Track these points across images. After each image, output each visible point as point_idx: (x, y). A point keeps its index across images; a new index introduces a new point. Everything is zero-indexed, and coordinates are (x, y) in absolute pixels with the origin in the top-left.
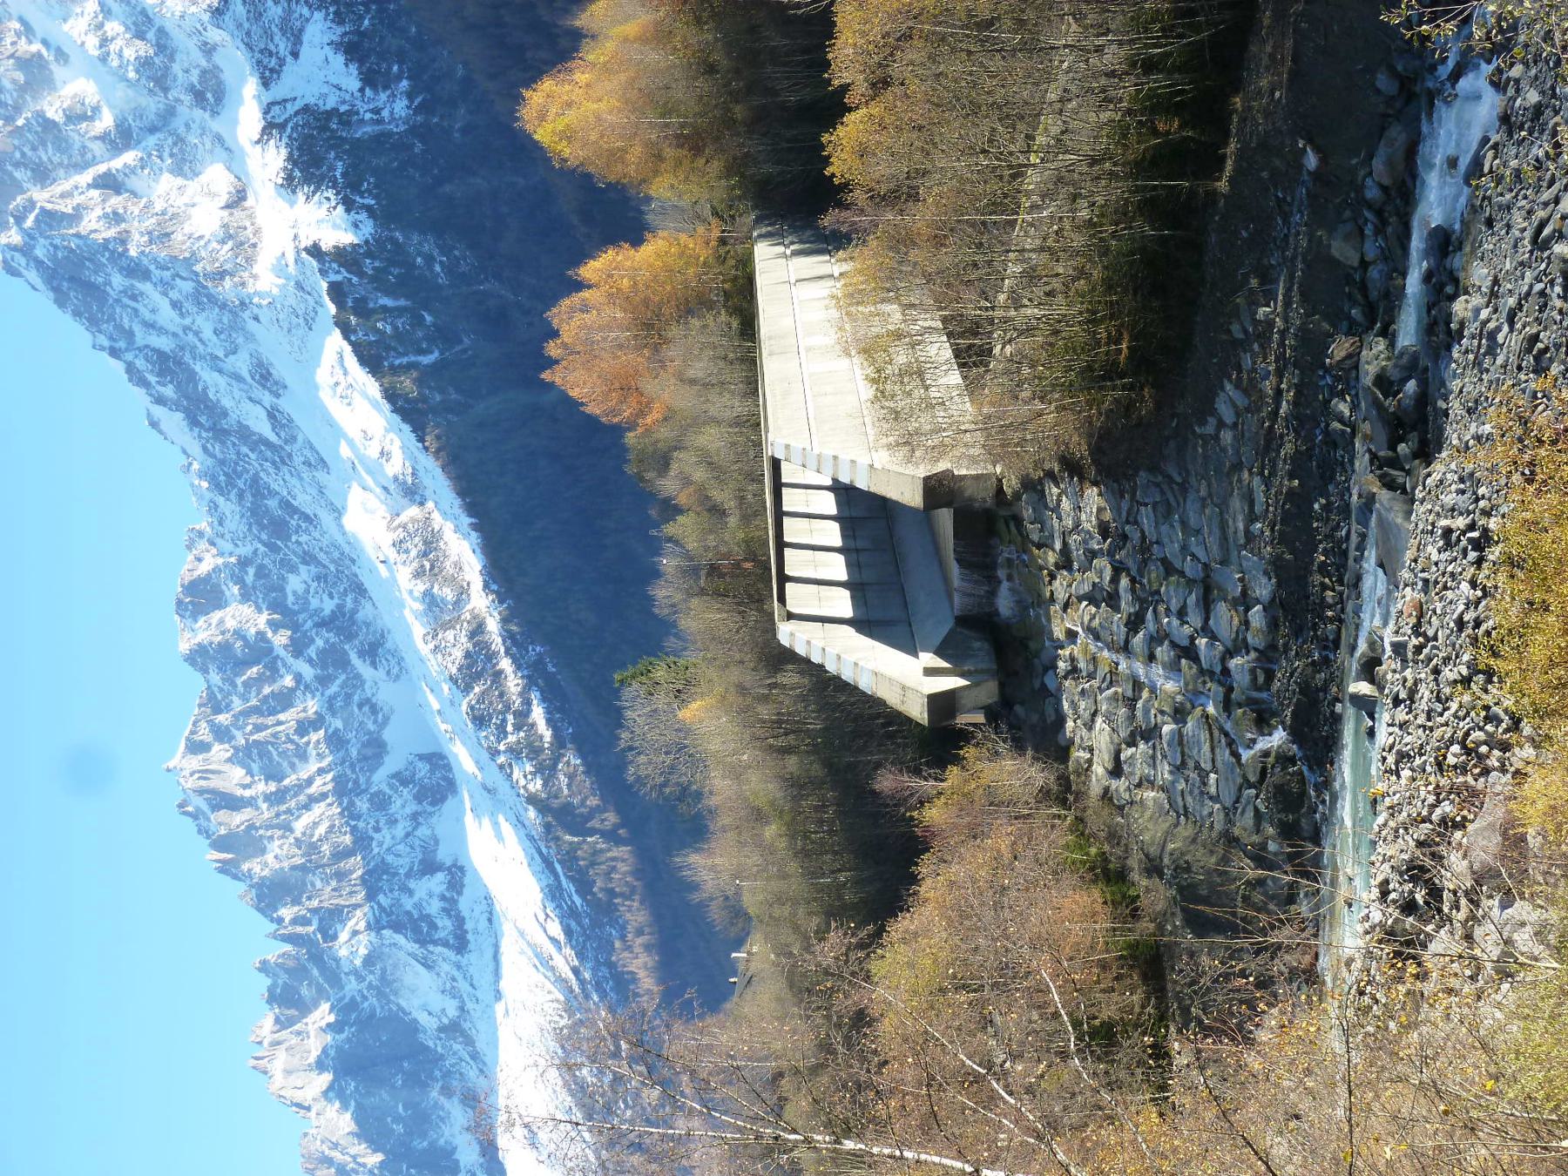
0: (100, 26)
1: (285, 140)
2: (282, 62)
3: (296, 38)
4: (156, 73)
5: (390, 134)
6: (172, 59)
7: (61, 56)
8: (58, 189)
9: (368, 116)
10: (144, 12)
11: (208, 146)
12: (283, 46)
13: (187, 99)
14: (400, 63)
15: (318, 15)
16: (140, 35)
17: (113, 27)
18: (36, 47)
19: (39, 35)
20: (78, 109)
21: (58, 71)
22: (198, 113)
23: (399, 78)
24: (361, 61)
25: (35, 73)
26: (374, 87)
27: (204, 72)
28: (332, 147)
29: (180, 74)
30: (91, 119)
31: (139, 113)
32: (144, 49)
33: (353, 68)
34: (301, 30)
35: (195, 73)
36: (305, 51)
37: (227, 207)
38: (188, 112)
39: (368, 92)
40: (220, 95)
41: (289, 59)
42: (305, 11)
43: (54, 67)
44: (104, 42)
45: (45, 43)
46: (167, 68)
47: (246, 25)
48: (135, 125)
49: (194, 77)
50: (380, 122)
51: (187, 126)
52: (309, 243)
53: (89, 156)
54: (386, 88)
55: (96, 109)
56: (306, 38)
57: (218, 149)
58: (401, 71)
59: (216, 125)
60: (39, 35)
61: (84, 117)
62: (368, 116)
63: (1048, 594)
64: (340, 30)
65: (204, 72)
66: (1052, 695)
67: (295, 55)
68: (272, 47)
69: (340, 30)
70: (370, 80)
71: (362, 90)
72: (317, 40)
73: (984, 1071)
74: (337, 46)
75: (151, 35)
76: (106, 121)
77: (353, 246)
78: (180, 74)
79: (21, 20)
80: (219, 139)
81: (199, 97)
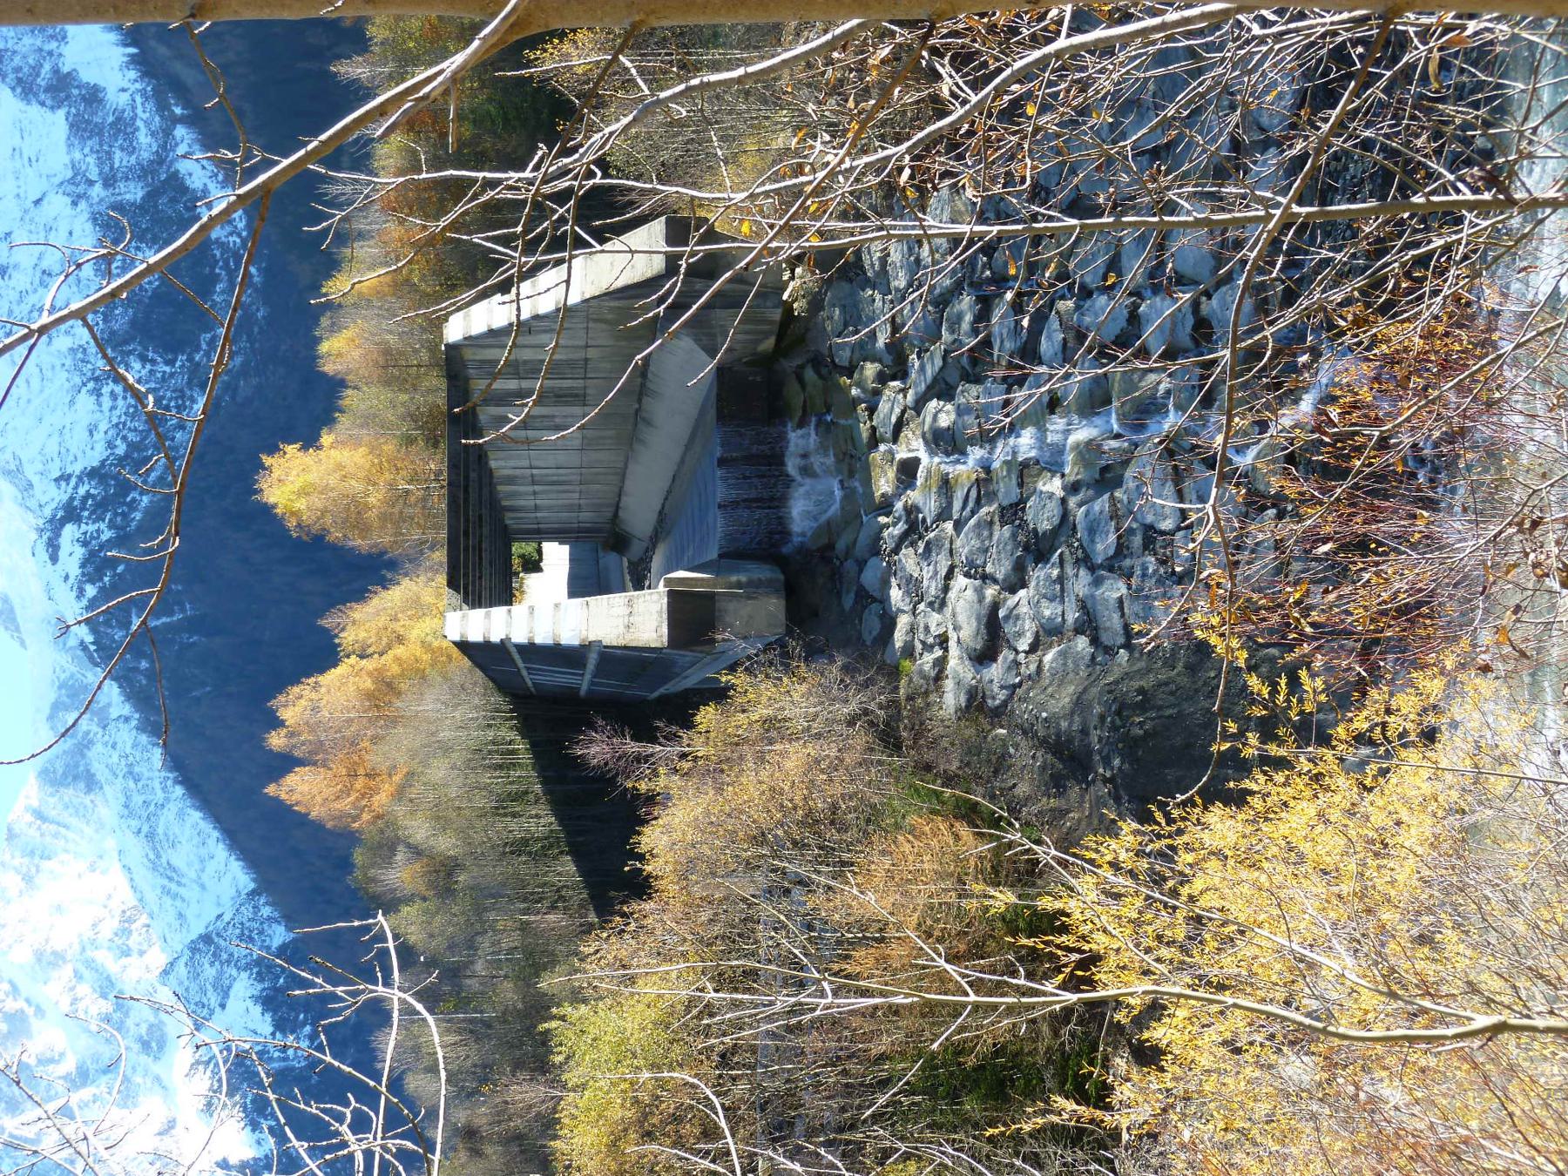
0: (72, 989)
1: (209, 1073)
2: (212, 1012)
3: (225, 993)
4: (114, 1022)
5: (293, 1069)
6: (127, 1014)
7: (40, 1011)
8: (24, 1118)
9: (276, 1054)
10: (108, 978)
11: (149, 1085)
12: (213, 999)
13: (136, 1047)
14: (306, 1012)
15: (244, 975)
16: (104, 996)
17: (84, 989)
18: (21, 1004)
19: (24, 995)
20: (48, 1055)
21: (35, 1024)
22: (143, 1059)
23: (304, 1024)
24: (275, 1011)
25: (18, 1024)
26: (283, 1032)
27: (151, 1026)
28: (245, 1080)
29: (133, 1027)
30: (58, 1062)
31: (96, 1058)
32: (106, 1006)
33: (268, 1017)
34: (229, 988)
35: (144, 1027)
36: (230, 1003)
37: (160, 1134)
38: (133, 1057)
39: (278, 1035)
40: (161, 1047)
41: (218, 1009)
42: (234, 972)
43: (32, 1020)
44: (75, 1001)
45: (28, 1001)
46: (122, 1022)
47: (186, 983)
48: (92, 1067)
49: (143, 1030)
50: (285, 1059)
51: (134, 1068)
52: (219, 1158)
53: (53, 1092)
54: (292, 1032)
55: (62, 1055)
56: (232, 993)
57: (157, 1087)
58: (306, 1018)
59: (156, 1068)
60: (24, 995)
61: (51, 1061)
62: (276, 1054)
63: (865, 435)
64: (260, 987)
65: (151, 1026)
66: (874, 600)
67: (223, 1006)
68: (205, 1000)
69: (260, 987)
70: (281, 1026)
71: (273, 1034)
72: (241, 994)
73: (455, 330)
74: (256, 999)
75: (111, 996)
76: (69, 1066)
77: (255, 1159)
78: (133, 1027)
79: (11, 982)
80: (158, 1079)
81: (145, 1045)
